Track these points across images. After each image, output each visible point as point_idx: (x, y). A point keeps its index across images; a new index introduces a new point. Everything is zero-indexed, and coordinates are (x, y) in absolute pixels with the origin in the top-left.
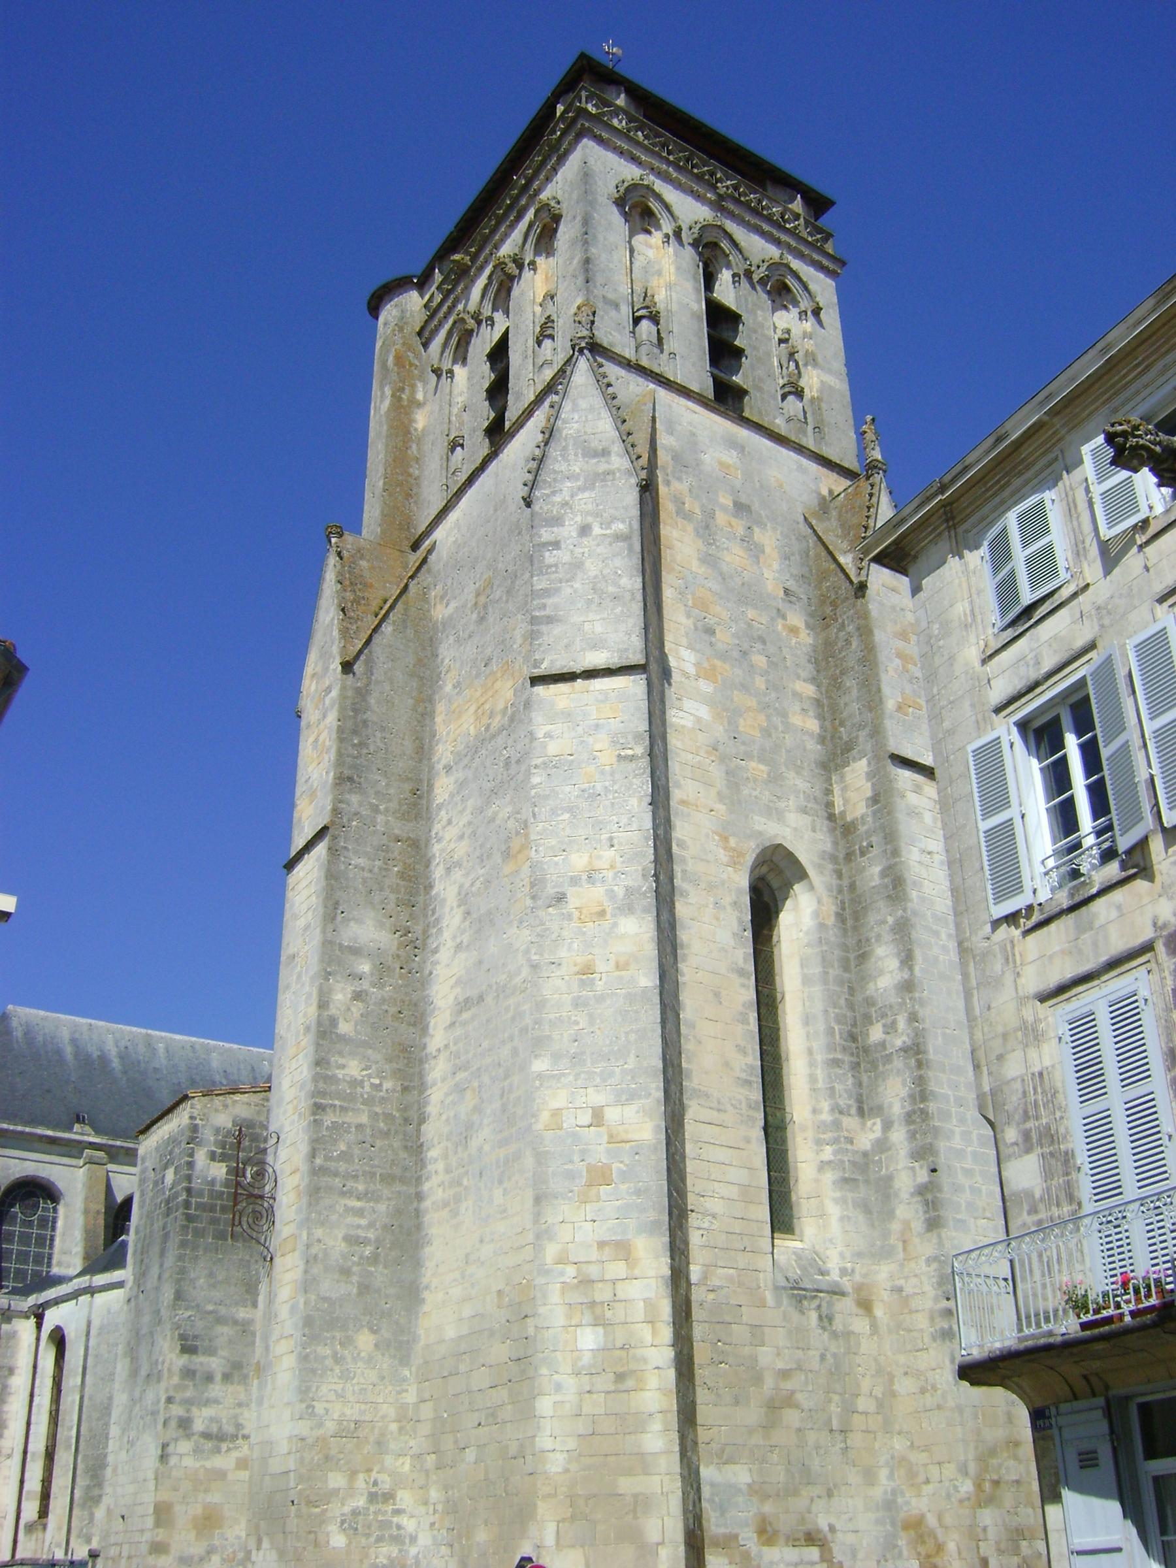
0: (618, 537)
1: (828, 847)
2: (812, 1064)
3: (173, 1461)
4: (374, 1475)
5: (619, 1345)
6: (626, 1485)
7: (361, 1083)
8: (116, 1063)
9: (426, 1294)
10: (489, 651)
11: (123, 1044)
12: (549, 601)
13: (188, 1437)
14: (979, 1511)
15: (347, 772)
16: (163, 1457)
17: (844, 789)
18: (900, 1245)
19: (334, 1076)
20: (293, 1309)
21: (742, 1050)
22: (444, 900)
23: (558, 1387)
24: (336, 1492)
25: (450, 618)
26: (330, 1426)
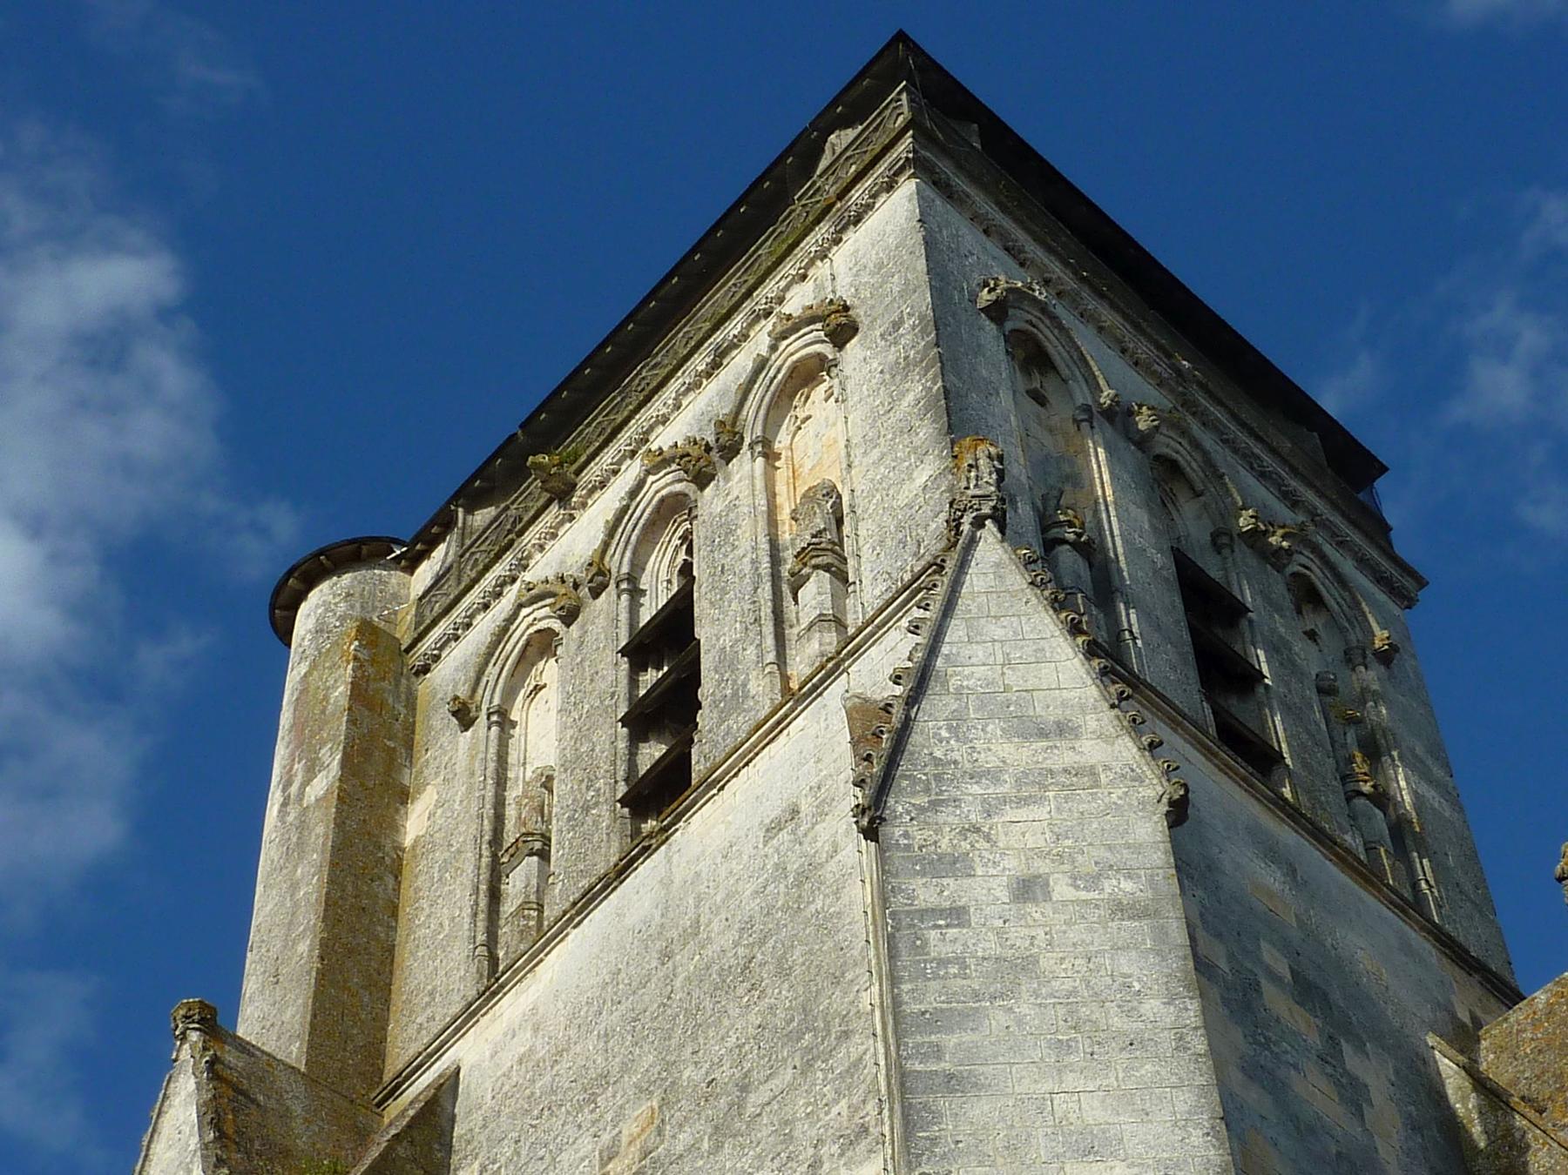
0: (1120, 909)
12: (950, 1041)
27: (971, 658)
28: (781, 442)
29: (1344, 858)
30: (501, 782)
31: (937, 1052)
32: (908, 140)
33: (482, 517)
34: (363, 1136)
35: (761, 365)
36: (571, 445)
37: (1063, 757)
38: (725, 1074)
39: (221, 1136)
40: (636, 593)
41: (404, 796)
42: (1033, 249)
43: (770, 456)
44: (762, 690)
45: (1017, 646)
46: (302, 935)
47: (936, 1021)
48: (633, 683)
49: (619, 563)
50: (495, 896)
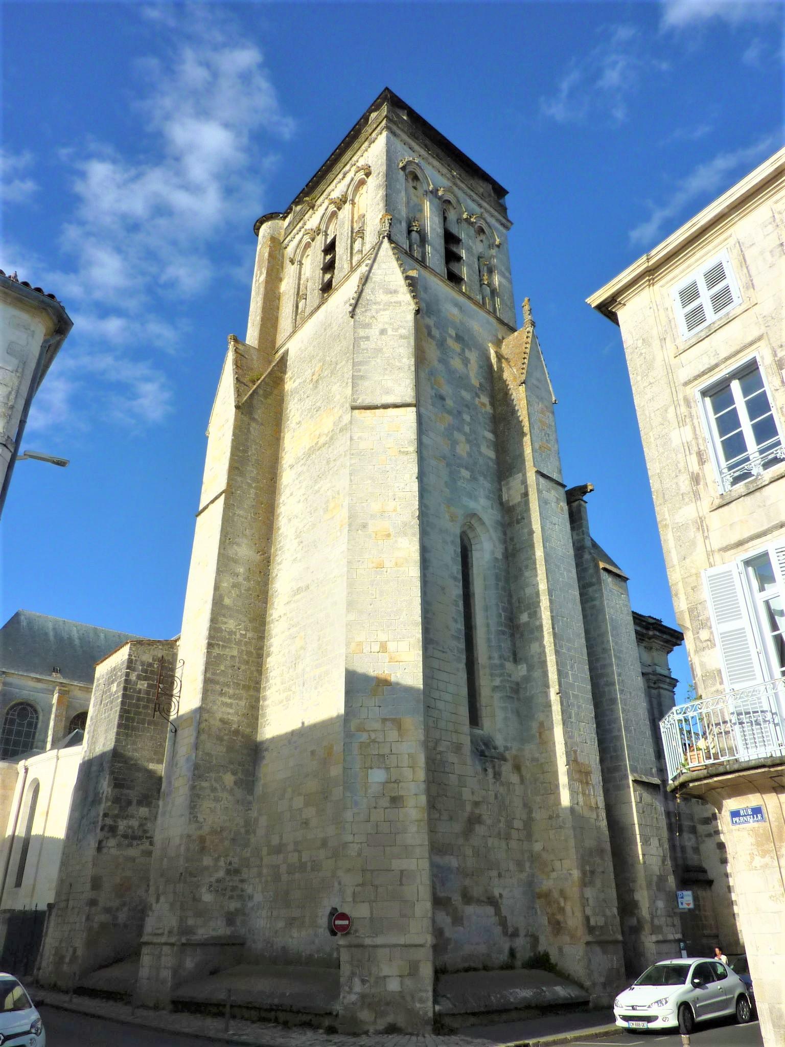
0: (401, 337)
1: (499, 518)
2: (488, 632)
3: (105, 850)
4: (229, 858)
5: (393, 780)
6: (397, 864)
7: (235, 633)
8: (77, 642)
9: (266, 754)
10: (318, 404)
11: (81, 632)
12: (363, 368)
13: (114, 836)
14: (585, 889)
15: (237, 465)
16: (99, 849)
17: (509, 489)
18: (538, 734)
19: (220, 628)
20: (188, 760)
21: (456, 621)
22: (286, 536)
23: (356, 803)
24: (207, 868)
25: (296, 388)
26: (206, 829)
27: (378, 274)
28: (356, 201)
29: (476, 303)
30: (299, 279)
31: (360, 370)
32: (385, 121)
33: (299, 208)
34: (270, 362)
35: (352, 180)
36: (313, 195)
37: (394, 298)
38: (334, 360)
39: (237, 366)
40: (326, 235)
41: (281, 280)
42: (417, 147)
43: (353, 203)
44: (346, 266)
45: (389, 271)
46: (398, 116)
47: (361, 363)
48: (325, 259)
49: (323, 227)
50: (297, 307)
